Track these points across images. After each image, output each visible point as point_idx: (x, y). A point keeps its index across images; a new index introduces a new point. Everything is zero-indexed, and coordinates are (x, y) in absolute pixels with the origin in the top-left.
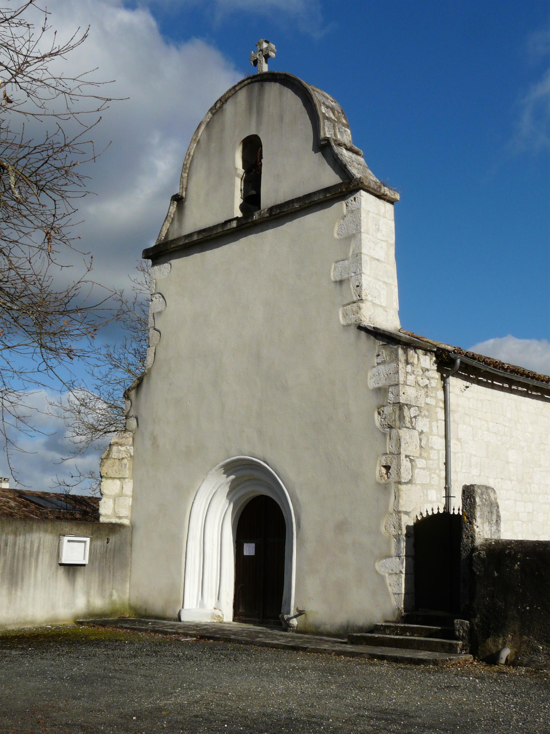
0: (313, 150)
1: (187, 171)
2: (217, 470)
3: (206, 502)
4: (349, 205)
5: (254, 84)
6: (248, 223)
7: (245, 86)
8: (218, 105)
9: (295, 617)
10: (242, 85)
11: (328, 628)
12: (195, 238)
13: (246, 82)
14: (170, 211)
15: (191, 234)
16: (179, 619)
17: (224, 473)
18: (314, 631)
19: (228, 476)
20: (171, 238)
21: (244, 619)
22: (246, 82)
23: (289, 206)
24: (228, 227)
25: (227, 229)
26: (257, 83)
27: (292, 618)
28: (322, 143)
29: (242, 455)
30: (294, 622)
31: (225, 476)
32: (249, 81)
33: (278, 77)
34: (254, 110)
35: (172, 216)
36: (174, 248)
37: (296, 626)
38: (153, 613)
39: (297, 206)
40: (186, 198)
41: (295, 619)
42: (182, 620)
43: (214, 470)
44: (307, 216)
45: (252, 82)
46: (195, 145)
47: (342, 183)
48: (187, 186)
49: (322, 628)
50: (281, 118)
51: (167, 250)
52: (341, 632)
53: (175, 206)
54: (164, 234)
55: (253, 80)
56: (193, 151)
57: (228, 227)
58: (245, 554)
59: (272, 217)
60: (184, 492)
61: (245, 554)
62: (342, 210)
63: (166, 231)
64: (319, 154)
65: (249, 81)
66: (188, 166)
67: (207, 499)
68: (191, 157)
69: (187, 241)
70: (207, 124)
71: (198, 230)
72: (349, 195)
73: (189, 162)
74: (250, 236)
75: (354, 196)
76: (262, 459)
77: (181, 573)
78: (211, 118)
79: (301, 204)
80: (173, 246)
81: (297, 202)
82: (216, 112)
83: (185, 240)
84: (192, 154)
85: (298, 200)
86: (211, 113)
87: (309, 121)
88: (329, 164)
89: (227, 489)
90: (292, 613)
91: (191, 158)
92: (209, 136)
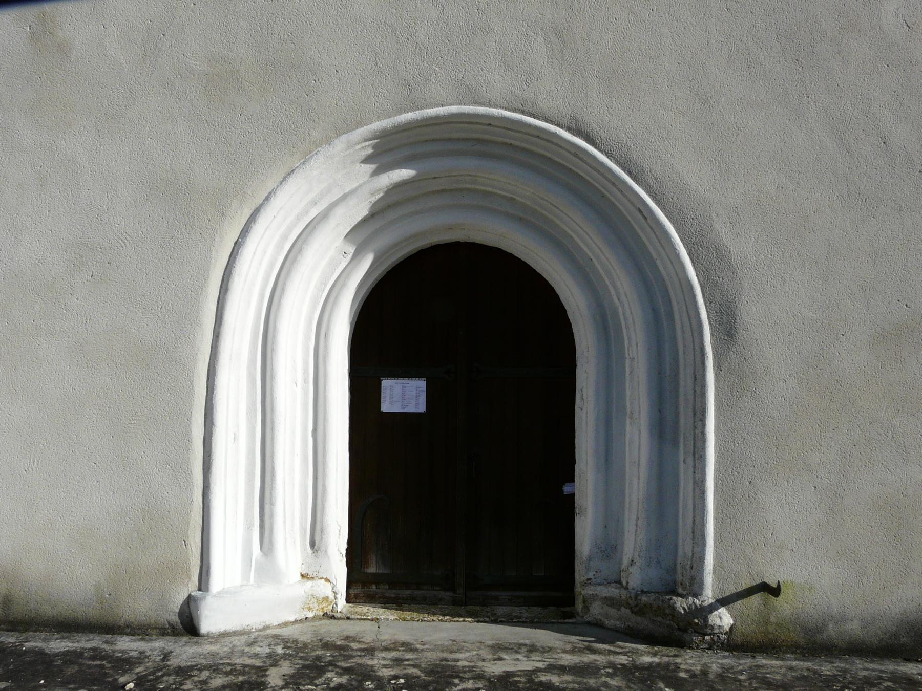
2: (350, 146)
3: (279, 247)
9: (724, 602)
11: (854, 628)
16: (188, 625)
17: (367, 160)
18: (802, 641)
19: (376, 173)
21: (392, 593)
27: (712, 608)
29: (476, 103)
30: (724, 619)
31: (370, 168)
37: (727, 628)
38: (48, 611)
41: (723, 611)
42: (206, 626)
43: (340, 144)
49: (832, 631)
52: (903, 640)
58: (386, 407)
60: (195, 213)
61: (386, 407)
67: (285, 237)
76: (565, 121)
77: (189, 475)
89: (363, 211)
90: (709, 594)
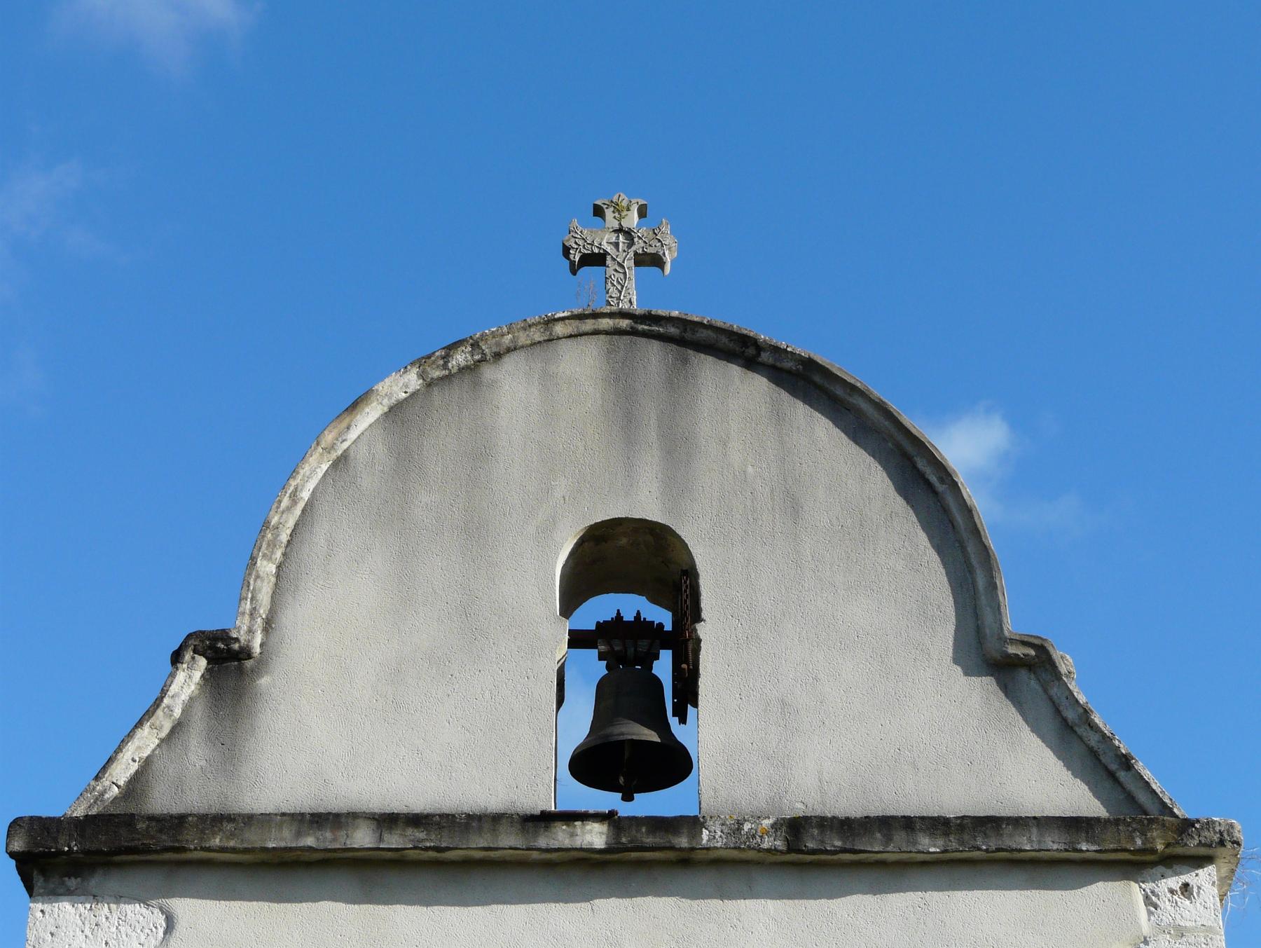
0: (956, 660)
1: (278, 555)
4: (1165, 903)
5: (642, 341)
6: (672, 848)
7: (596, 332)
8: (460, 358)
10: (589, 325)
12: (363, 838)
13: (606, 323)
14: (174, 688)
15: (337, 816)
20: (162, 801)
22: (606, 323)
23: (888, 839)
24: (561, 837)
25: (554, 844)
26: (655, 345)
28: (1012, 650)
32: (624, 323)
33: (765, 357)
34: (651, 433)
35: (177, 713)
36: (223, 850)
39: (931, 846)
40: (263, 664)
44: (959, 895)
45: (633, 332)
46: (325, 467)
47: (1107, 821)
48: (271, 611)
50: (793, 507)
51: (184, 850)
53: (197, 675)
54: (122, 772)
55: (641, 327)
56: (311, 485)
57: (561, 837)
59: (793, 857)
62: (1136, 921)
63: (134, 767)
64: (988, 682)
65: (624, 323)
66: (284, 537)
68: (301, 505)
69: (310, 841)
70: (391, 409)
71: (935, 813)
72: (1161, 869)
73: (291, 523)
74: (650, 899)
75: (1185, 878)
78: (413, 395)
79: (954, 845)
80: (217, 842)
81: (932, 835)
82: (441, 379)
83: (299, 834)
84: (305, 495)
85: (938, 825)
86: (421, 376)
87: (932, 557)
88: (1035, 729)
91: (298, 511)
92: (405, 461)
